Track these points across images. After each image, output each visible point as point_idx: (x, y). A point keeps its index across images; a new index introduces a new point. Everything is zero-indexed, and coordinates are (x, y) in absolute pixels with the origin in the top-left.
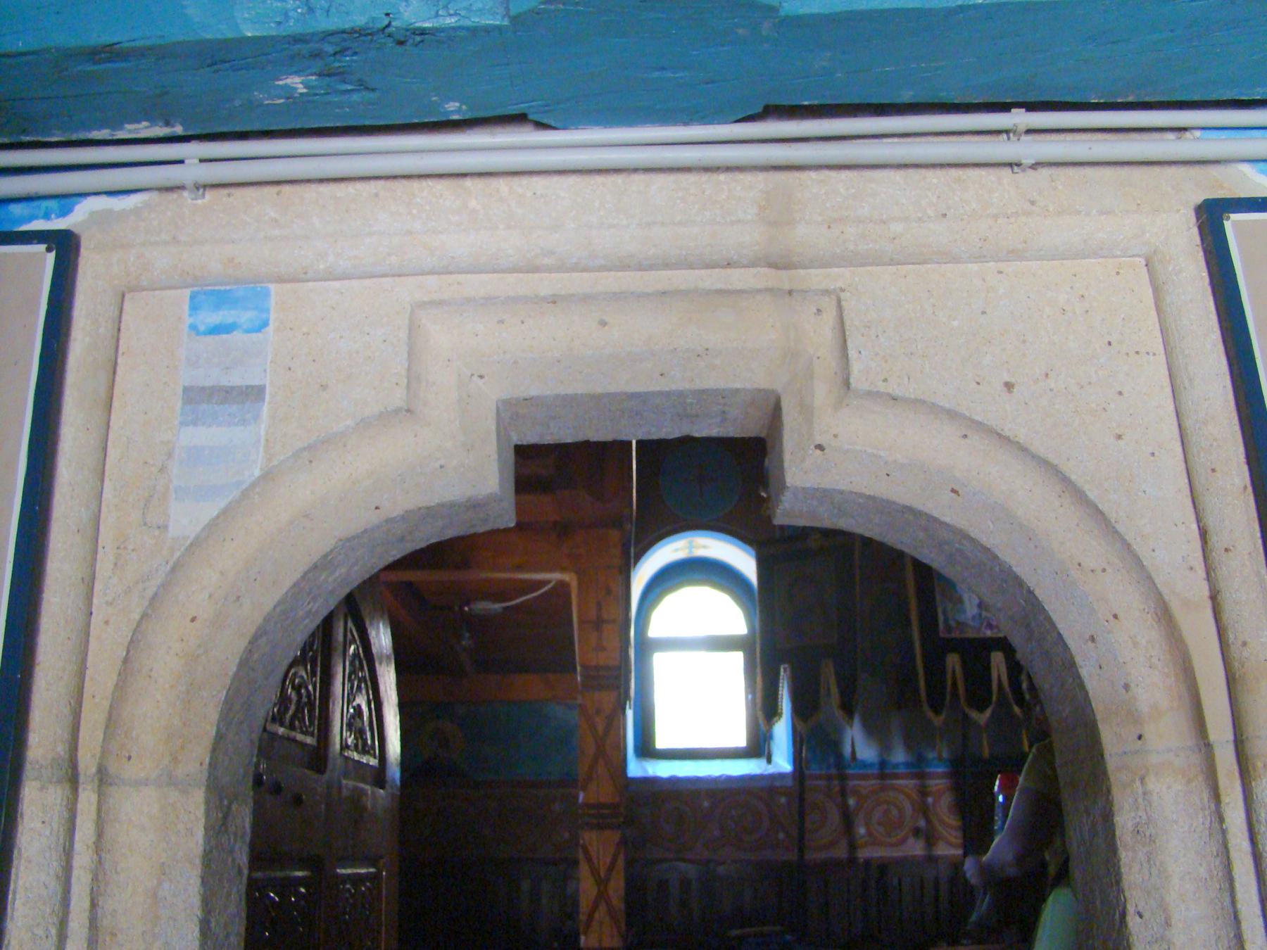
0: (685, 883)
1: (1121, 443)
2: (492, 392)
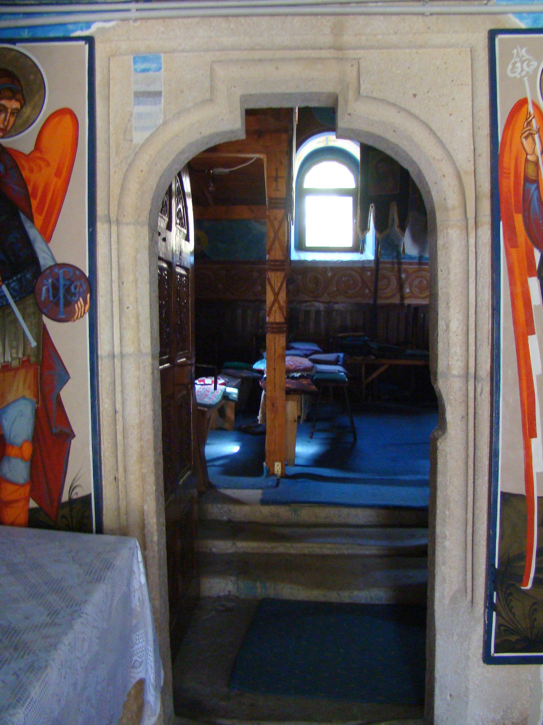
0: (318, 312)
2: (239, 92)
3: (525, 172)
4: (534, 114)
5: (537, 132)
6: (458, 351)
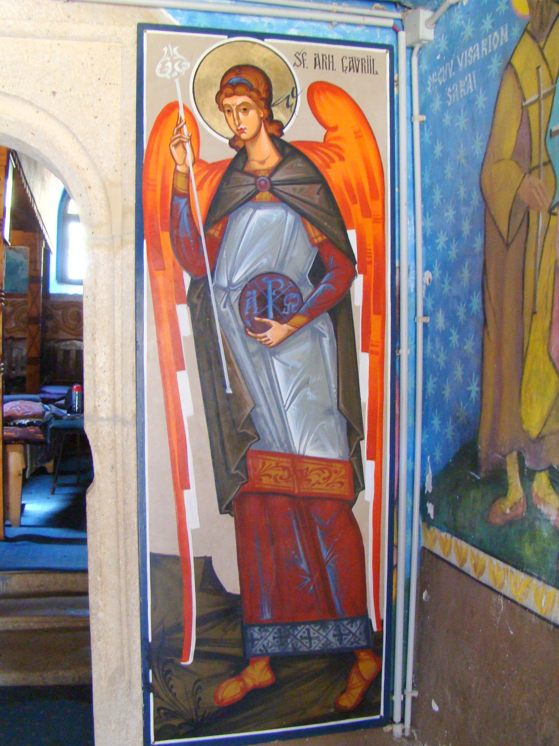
1: (96, 120)
3: (173, 185)
4: (185, 119)
5: (189, 140)
6: (106, 389)
